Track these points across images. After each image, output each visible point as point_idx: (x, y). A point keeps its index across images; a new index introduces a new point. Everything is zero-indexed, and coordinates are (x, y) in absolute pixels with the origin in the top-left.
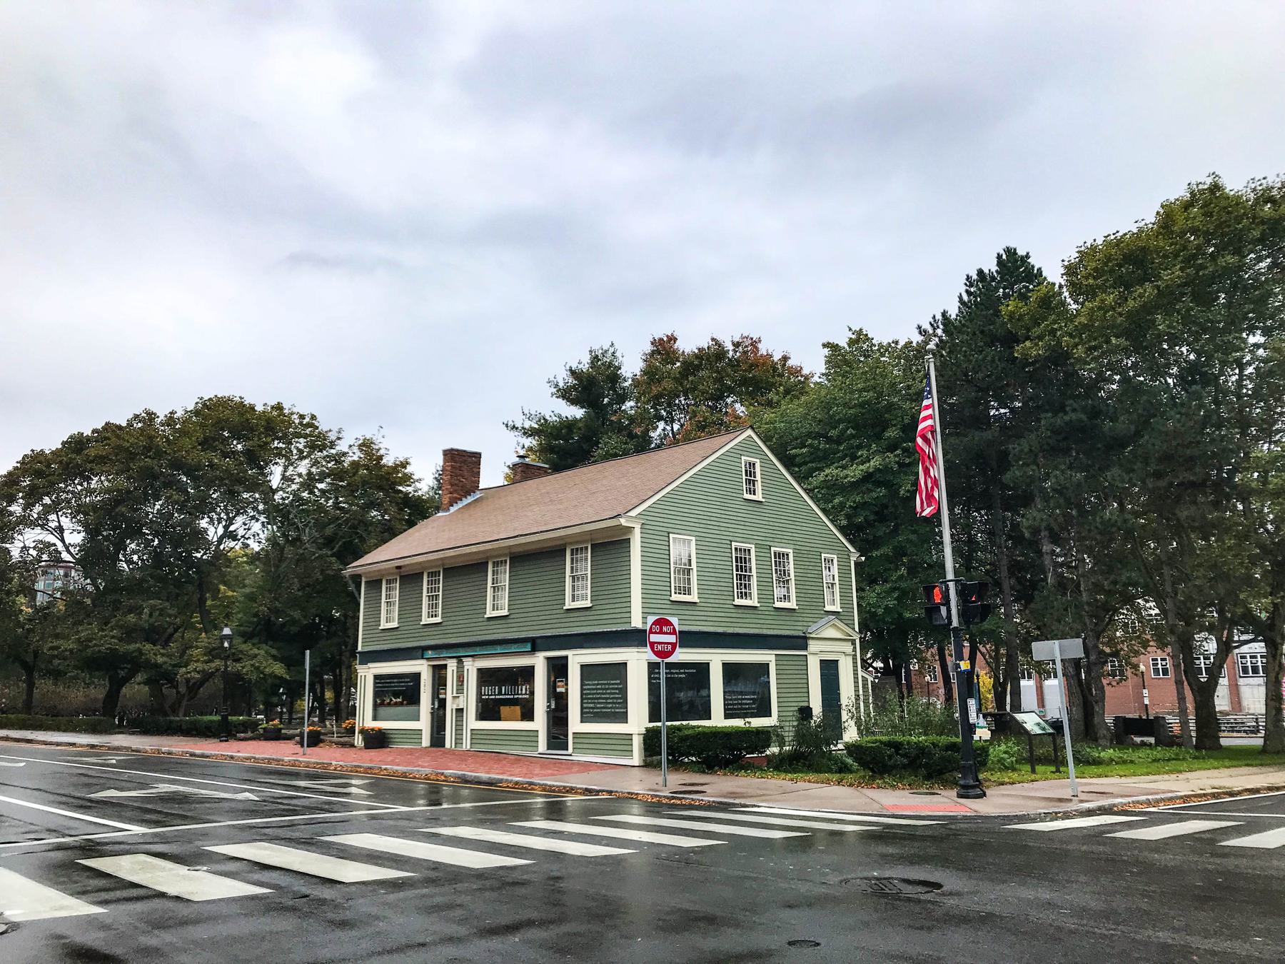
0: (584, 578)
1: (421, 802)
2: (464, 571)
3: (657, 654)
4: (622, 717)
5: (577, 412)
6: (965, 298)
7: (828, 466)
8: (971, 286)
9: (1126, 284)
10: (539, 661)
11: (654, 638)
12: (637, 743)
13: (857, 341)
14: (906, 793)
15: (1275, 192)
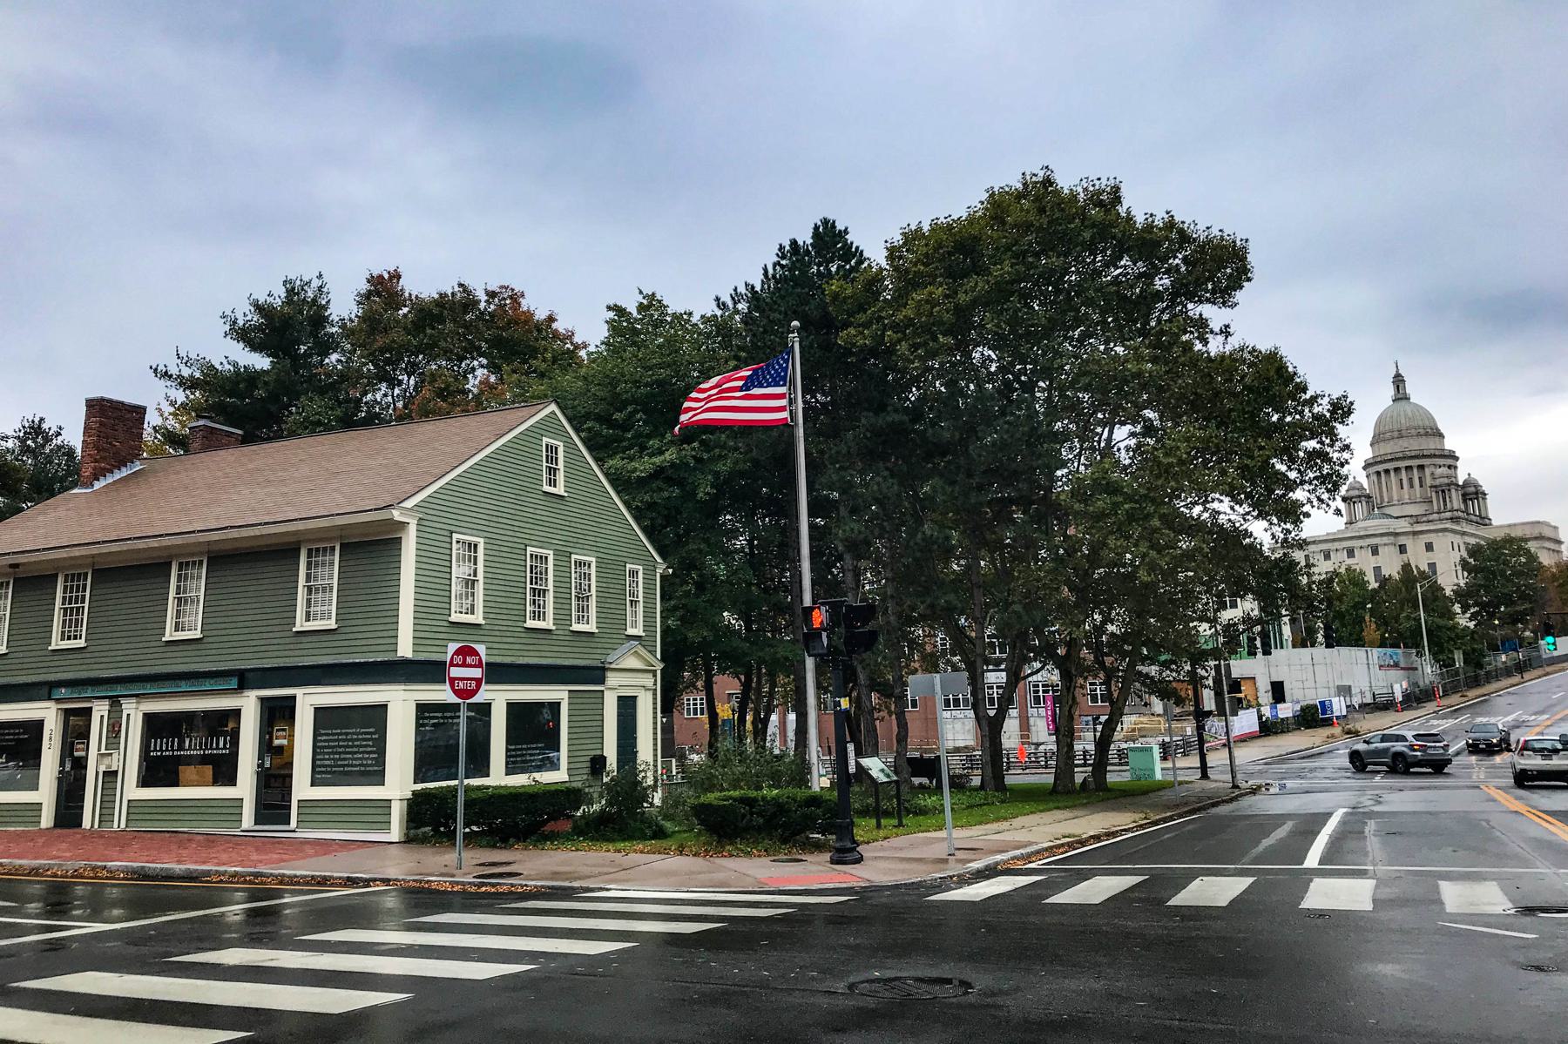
0: (326, 589)
1: (116, 912)
2: (134, 574)
3: (457, 693)
5: (261, 362)
6: (771, 271)
7: (611, 457)
8: (783, 257)
9: (955, 275)
10: (249, 705)
11: (455, 672)
12: (397, 813)
13: (650, 305)
14: (766, 861)
15: (1104, 197)
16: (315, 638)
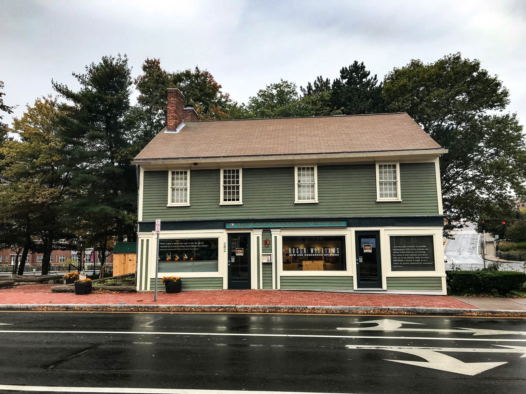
4: (432, 267)
16: (395, 205)
